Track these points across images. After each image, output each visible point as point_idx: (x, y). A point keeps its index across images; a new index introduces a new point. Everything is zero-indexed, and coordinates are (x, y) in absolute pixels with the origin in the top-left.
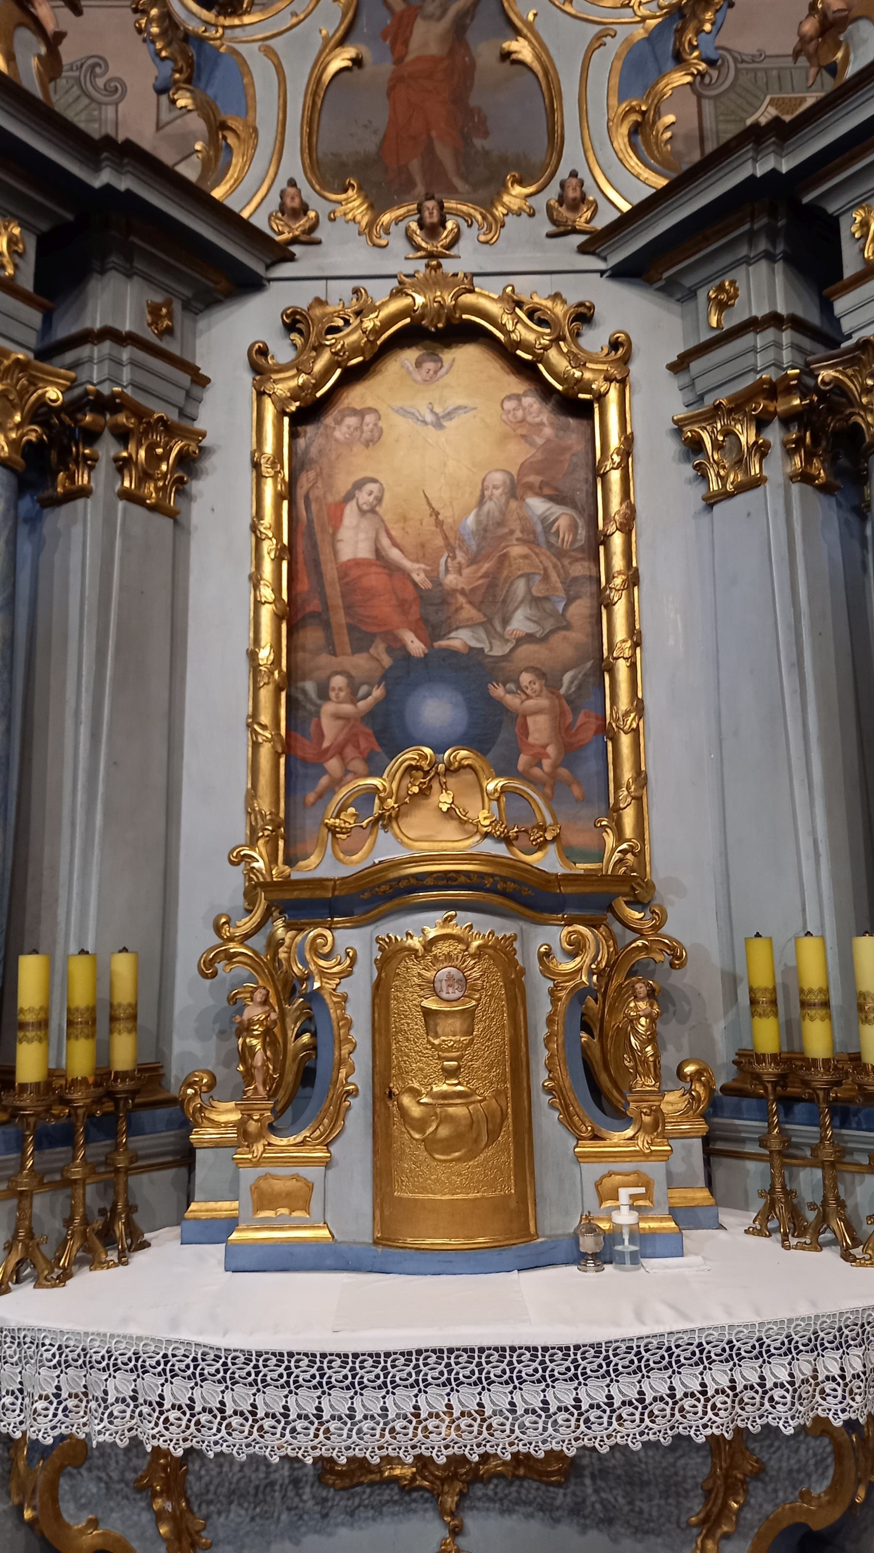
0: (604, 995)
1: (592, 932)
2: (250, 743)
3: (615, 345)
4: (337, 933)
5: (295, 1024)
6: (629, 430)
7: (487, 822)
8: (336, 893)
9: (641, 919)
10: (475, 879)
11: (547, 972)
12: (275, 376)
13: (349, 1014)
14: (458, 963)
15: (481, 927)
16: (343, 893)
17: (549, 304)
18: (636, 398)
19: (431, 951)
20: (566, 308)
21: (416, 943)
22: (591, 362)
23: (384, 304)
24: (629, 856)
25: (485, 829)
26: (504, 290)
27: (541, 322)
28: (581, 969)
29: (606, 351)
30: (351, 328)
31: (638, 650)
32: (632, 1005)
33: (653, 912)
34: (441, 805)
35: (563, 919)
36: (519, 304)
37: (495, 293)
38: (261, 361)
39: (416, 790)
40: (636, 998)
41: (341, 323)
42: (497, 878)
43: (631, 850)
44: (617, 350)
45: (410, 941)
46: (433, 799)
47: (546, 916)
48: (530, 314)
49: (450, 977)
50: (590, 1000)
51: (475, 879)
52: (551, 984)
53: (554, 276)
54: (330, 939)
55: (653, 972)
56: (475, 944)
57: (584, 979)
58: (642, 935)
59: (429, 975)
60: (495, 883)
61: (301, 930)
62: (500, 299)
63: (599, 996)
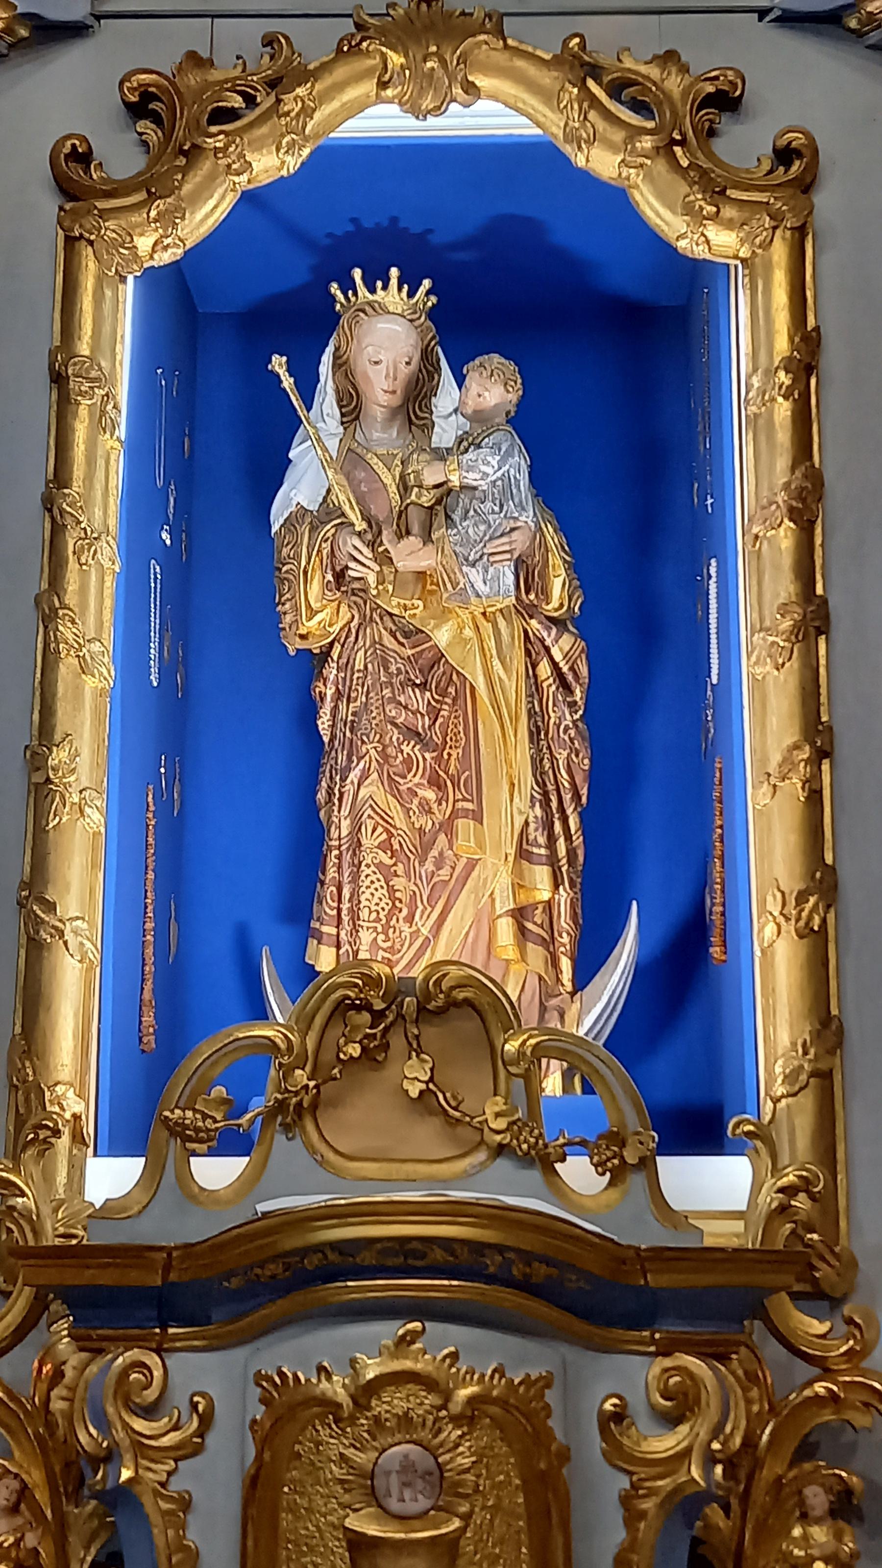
0: (745, 1498)
1: (712, 1368)
2: (24, 941)
3: (784, 155)
4: (173, 1360)
5: (87, 1548)
6: (811, 322)
7: (501, 1124)
8: (173, 1277)
9: (823, 1336)
10: (464, 1254)
11: (618, 1455)
12: (101, 204)
13: (193, 1537)
14: (424, 1435)
15: (475, 1359)
16: (186, 1277)
17: (654, 72)
18: (828, 260)
19: (369, 1408)
20: (687, 80)
21: (337, 1388)
22: (737, 186)
23: (325, 67)
24: (801, 1202)
25: (498, 1138)
26: (565, 42)
27: (639, 107)
28: (686, 1453)
29: (766, 166)
30: (258, 111)
31: (826, 766)
32: (797, 1532)
33: (850, 1321)
34: (406, 1085)
35: (653, 1341)
36: (595, 71)
37: (547, 51)
38: (76, 171)
39: (354, 1050)
40: (804, 1518)
41: (237, 102)
42: (511, 1255)
43: (805, 1185)
44: (788, 165)
45: (325, 1385)
46: (390, 1072)
47: (619, 1333)
48: (616, 90)
49: (407, 1466)
50: (715, 1513)
51: (464, 1254)
52: (624, 1482)
53: (663, 17)
54: (158, 1373)
55: (852, 1448)
56: (464, 1393)
57: (695, 1473)
58: (827, 1370)
59: (361, 1458)
60: (508, 1264)
61: (100, 1352)
62: (557, 62)
63: (734, 1502)
